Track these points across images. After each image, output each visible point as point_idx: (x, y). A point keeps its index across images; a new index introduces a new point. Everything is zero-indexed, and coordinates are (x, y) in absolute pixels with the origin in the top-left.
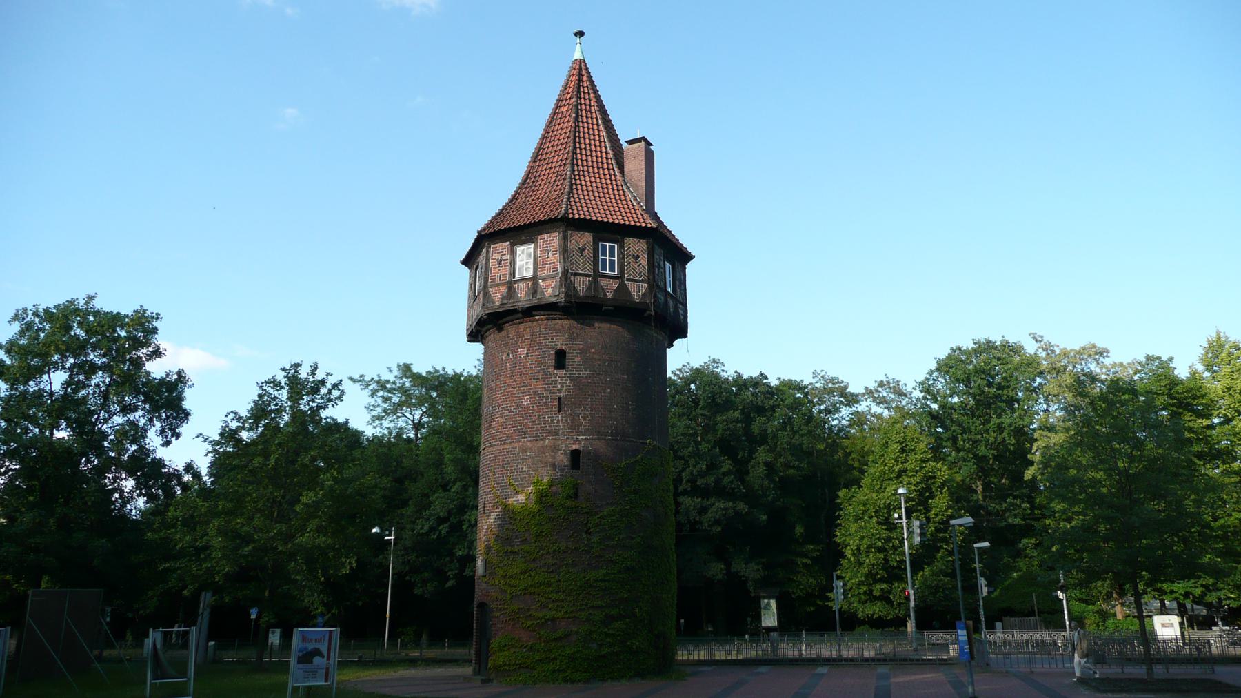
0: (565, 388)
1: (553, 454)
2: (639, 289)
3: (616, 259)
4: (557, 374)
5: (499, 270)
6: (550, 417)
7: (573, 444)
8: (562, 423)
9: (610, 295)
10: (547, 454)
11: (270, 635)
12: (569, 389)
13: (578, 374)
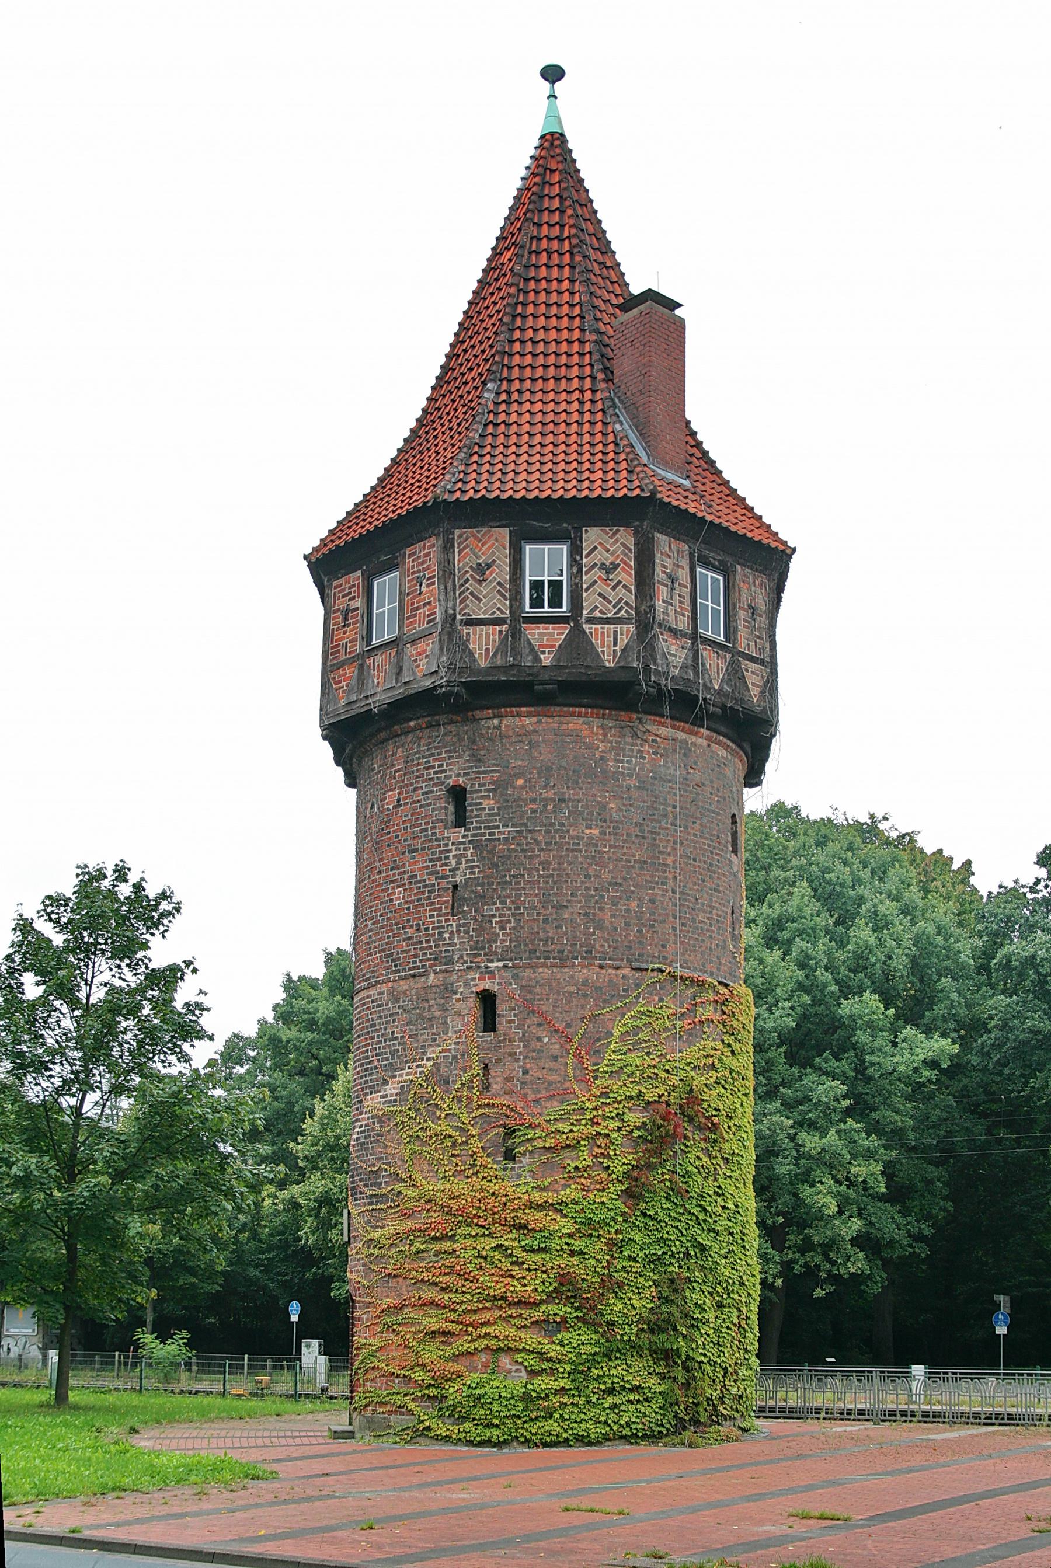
0: (463, 866)
1: (443, 1001)
2: (615, 639)
3: (564, 578)
4: (449, 838)
5: (344, 633)
6: (438, 928)
7: (480, 979)
8: (460, 938)
9: (546, 660)
10: (432, 1002)
11: (304, 1349)
12: (472, 867)
13: (490, 834)
